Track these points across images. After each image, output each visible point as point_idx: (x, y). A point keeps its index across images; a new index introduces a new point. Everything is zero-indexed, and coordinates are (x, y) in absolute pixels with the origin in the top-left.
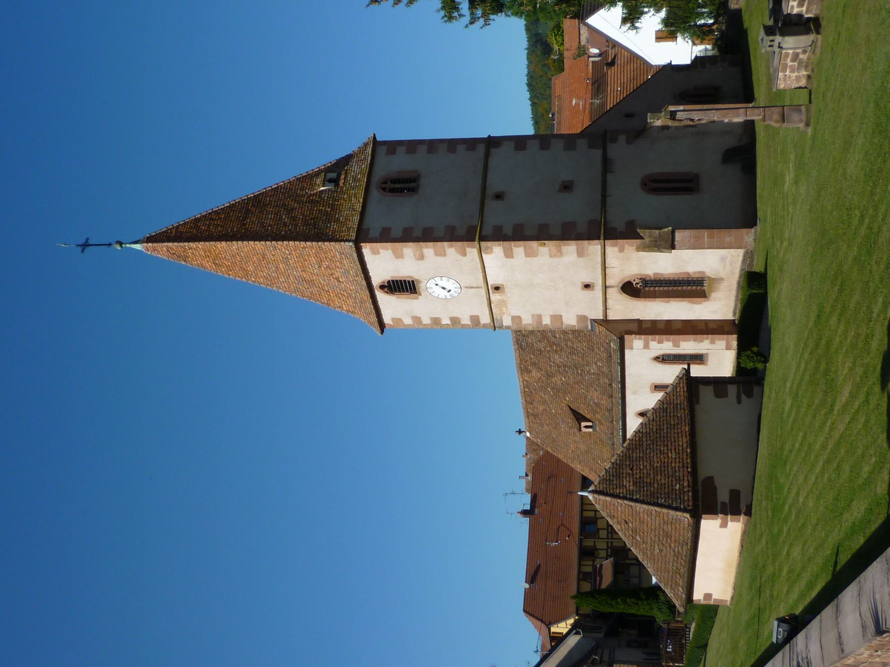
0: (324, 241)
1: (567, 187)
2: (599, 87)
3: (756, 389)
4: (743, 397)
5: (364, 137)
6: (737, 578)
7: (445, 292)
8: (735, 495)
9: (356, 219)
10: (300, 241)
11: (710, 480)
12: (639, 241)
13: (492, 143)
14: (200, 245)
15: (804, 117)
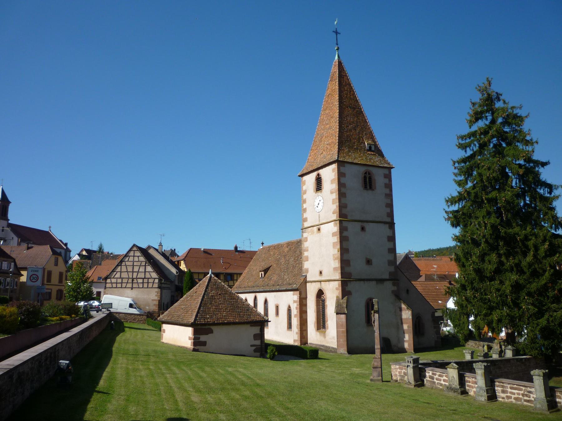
0: (339, 145)
1: (369, 262)
2: (443, 278)
3: (258, 354)
4: (254, 348)
5: (393, 163)
6: (171, 345)
7: (317, 205)
8: (204, 344)
9: (350, 160)
10: (339, 134)
11: (212, 332)
12: (341, 297)
13: (391, 225)
14: (337, 87)
15: (375, 378)
